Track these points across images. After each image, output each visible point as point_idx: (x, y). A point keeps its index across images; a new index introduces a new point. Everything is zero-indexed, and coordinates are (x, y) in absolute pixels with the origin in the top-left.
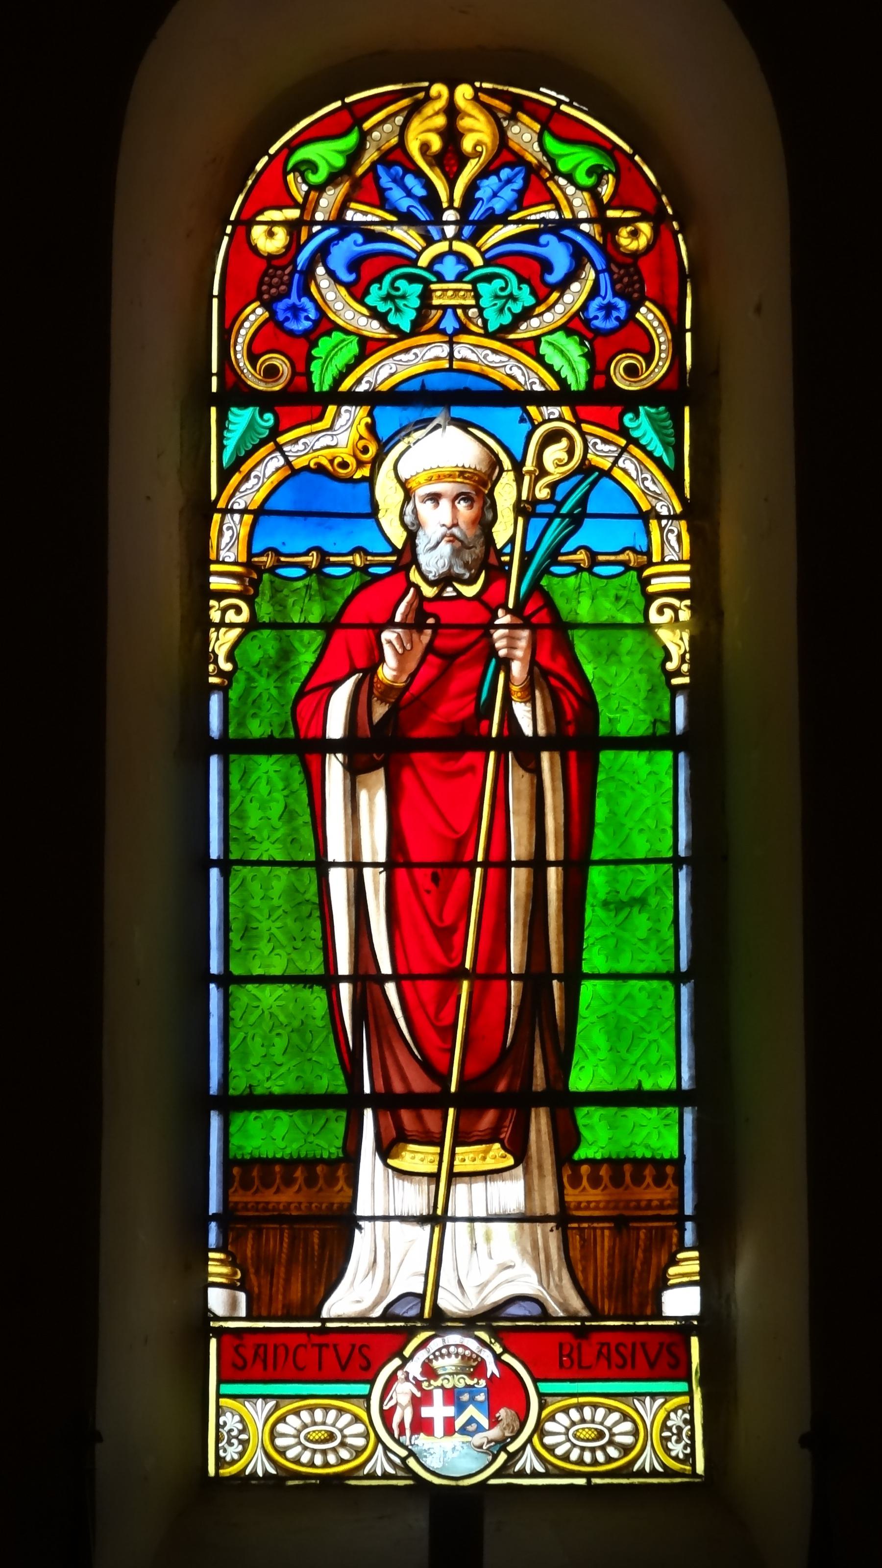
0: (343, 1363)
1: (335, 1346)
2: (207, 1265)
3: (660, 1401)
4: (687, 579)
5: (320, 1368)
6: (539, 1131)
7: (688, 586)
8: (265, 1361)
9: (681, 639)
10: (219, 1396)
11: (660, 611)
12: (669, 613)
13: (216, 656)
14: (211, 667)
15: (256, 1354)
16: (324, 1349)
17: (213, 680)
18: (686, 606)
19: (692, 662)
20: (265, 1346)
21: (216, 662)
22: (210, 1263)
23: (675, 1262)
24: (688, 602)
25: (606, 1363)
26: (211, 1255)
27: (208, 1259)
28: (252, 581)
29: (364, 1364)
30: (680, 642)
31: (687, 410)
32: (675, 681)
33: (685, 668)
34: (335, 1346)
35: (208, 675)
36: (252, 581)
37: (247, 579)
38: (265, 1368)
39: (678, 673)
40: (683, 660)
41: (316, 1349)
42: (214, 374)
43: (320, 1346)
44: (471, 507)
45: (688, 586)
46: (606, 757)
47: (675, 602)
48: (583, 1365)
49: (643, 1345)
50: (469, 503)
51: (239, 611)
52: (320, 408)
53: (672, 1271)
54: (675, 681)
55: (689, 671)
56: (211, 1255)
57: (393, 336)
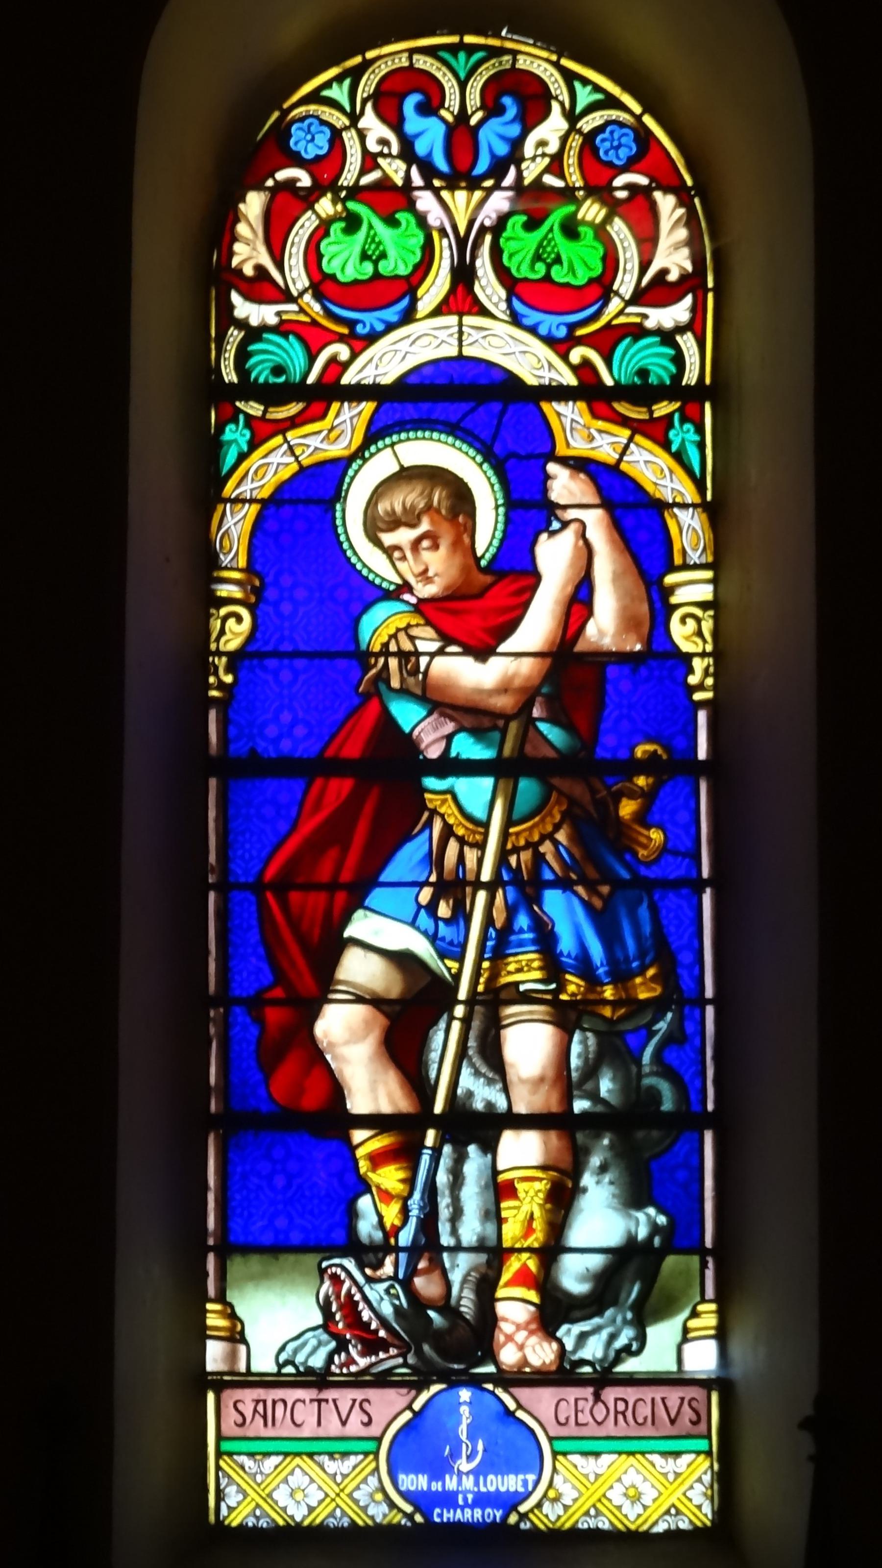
0: (344, 1418)
1: (334, 1401)
2: (205, 1318)
3: (289, 1459)
4: (710, 588)
5: (319, 1423)
6: (298, 358)
8: (265, 1417)
10: (219, 1454)
11: (683, 620)
12: (691, 624)
13: (216, 668)
14: (212, 680)
15: (255, 1411)
16: (323, 1404)
17: (214, 693)
18: (710, 616)
19: (716, 675)
20: (265, 1402)
21: (216, 674)
22: (208, 1315)
24: (711, 613)
25: (261, 1421)
26: (209, 1306)
27: (206, 1311)
28: (254, 588)
29: (694, 1418)
31: (708, 407)
33: (710, 681)
34: (334, 1401)
35: (209, 687)
36: (254, 588)
37: (249, 587)
38: (266, 1424)
39: (701, 687)
40: (706, 673)
41: (316, 1404)
42: (461, 1002)
43: (320, 1401)
46: (623, 467)
47: (698, 612)
51: (239, 619)
52: (325, 381)
54: (698, 696)
56: (209, 1306)
57: (405, 302)
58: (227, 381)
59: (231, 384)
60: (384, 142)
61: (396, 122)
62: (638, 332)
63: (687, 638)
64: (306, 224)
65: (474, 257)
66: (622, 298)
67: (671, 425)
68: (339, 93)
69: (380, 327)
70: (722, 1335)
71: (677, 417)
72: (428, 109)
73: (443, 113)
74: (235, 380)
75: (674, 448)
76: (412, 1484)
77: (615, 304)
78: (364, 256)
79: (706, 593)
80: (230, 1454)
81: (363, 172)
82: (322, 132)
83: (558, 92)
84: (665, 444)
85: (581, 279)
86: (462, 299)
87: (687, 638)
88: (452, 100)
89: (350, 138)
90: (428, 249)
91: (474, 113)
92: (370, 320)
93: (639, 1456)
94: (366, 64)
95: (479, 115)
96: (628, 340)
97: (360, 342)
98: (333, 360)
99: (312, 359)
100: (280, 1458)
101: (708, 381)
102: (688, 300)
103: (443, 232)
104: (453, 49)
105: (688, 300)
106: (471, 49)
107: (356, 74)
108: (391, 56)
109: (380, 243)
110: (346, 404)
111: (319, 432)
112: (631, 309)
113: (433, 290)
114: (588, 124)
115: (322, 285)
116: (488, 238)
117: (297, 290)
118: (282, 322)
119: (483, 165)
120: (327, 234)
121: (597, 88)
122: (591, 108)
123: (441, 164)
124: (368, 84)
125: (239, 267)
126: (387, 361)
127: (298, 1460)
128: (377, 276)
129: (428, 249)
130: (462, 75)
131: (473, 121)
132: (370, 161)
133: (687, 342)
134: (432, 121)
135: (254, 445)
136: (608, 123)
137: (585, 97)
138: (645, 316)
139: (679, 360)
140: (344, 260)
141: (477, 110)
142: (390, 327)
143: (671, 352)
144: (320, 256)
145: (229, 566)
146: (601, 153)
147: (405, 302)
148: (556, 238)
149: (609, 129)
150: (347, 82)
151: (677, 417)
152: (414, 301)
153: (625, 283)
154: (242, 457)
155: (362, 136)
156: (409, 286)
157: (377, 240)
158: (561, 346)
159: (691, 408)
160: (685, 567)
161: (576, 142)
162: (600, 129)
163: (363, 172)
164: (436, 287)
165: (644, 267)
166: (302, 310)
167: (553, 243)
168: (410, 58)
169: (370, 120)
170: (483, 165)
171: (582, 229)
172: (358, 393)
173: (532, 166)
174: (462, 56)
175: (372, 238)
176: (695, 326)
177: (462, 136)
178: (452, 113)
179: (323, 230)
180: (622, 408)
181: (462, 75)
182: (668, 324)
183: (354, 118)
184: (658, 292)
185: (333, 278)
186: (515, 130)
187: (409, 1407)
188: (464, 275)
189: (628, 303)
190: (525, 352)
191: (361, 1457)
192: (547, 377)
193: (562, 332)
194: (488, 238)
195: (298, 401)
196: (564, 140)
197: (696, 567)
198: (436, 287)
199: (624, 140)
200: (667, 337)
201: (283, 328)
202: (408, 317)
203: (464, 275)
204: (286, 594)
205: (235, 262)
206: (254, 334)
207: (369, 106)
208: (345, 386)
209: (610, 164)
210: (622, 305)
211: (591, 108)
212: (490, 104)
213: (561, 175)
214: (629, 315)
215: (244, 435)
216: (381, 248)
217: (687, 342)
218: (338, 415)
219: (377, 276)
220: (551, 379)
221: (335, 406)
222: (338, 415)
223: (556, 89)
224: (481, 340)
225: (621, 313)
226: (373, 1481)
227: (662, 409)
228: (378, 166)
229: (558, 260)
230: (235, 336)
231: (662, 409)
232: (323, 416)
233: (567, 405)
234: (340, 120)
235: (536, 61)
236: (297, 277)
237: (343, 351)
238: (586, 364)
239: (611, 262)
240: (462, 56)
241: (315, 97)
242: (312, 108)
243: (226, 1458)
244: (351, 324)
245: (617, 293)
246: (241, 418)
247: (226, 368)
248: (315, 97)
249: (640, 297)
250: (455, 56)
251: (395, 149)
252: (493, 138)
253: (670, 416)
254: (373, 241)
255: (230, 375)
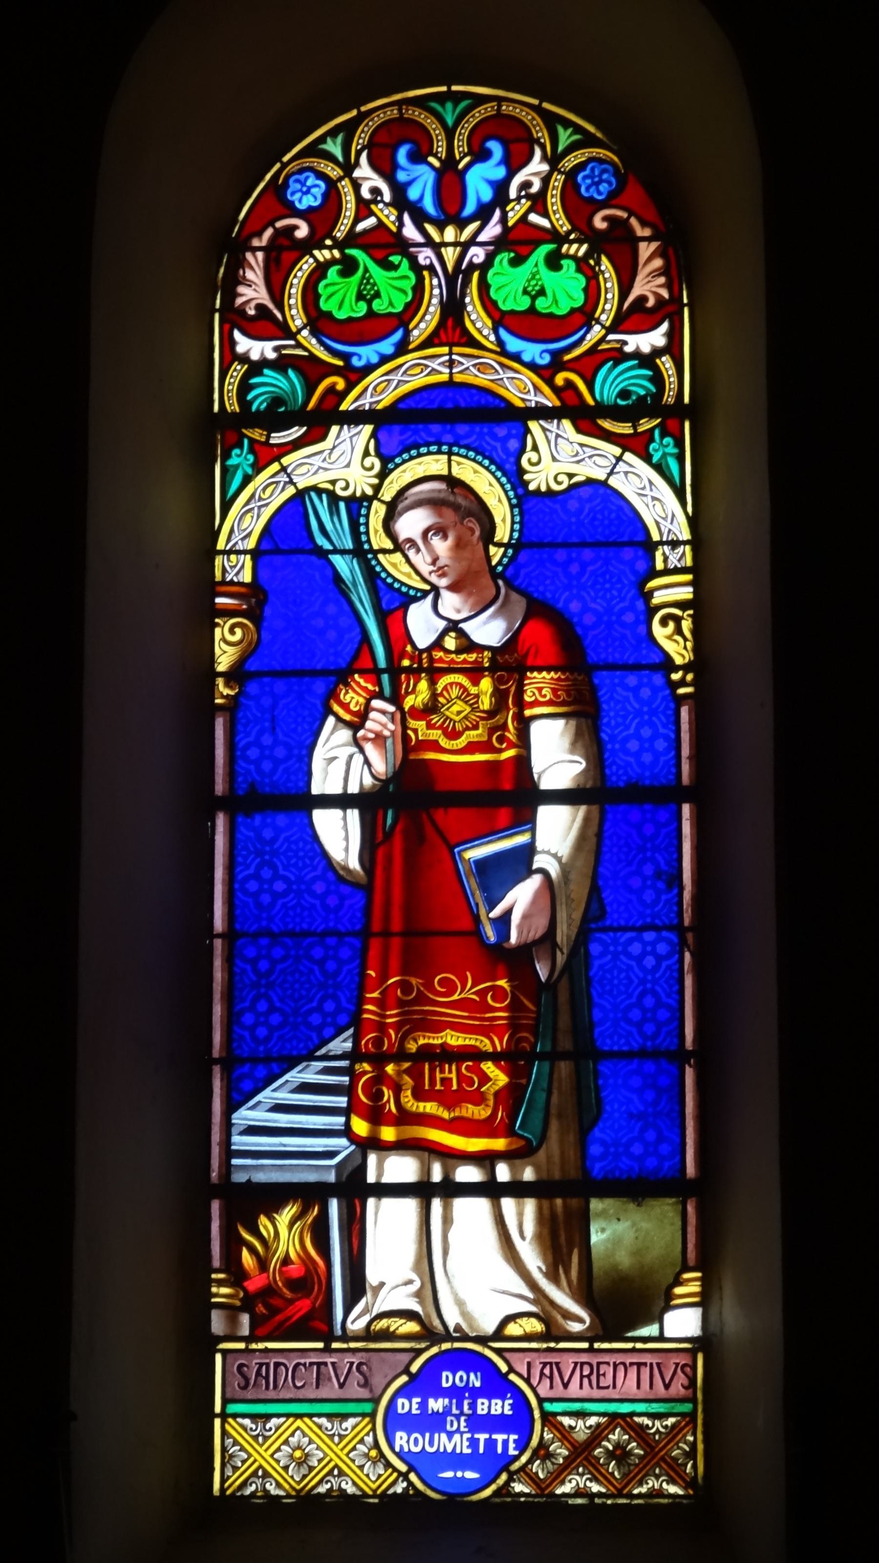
3: (291, 1420)
4: (691, 589)
7: (691, 596)
8: (267, 1378)
9: (685, 648)
15: (542, 1374)
16: (322, 1367)
17: (218, 701)
23: (678, 1282)
30: (684, 652)
32: (682, 691)
39: (683, 683)
41: (635, 1367)
44: (445, 537)
45: (691, 596)
48: (601, 1385)
49: (658, 1364)
50: (441, 534)
53: (678, 1290)
54: (682, 691)
55: (693, 680)
57: (398, 336)
58: (229, 410)
59: (234, 413)
60: (376, 191)
61: (386, 168)
62: (619, 356)
63: (669, 638)
64: (306, 265)
65: (463, 295)
66: (603, 326)
67: (652, 440)
68: (334, 147)
69: (375, 359)
70: (704, 1301)
71: (657, 433)
72: (418, 157)
73: (431, 159)
74: (238, 410)
75: (655, 460)
76: (416, 1440)
77: (597, 331)
78: (360, 297)
79: (686, 593)
80: (235, 1416)
81: (357, 220)
82: (315, 198)
83: (540, 134)
84: (647, 458)
85: (562, 310)
86: (452, 330)
87: (669, 638)
88: (441, 148)
89: (345, 186)
90: (419, 289)
91: (461, 159)
92: (366, 354)
93: (306, 1420)
94: (362, 117)
95: (467, 159)
96: (610, 364)
97: (355, 375)
98: (331, 389)
99: (309, 392)
100: (359, 1419)
101: (687, 400)
102: (665, 327)
103: (431, 268)
104: (440, 98)
105: (665, 327)
106: (457, 97)
107: (349, 129)
108: (381, 108)
109: (375, 284)
110: (345, 427)
111: (321, 452)
112: (611, 337)
113: (422, 325)
114: (570, 162)
115: (320, 322)
116: (476, 275)
117: (296, 326)
118: (281, 357)
119: (470, 207)
120: (324, 276)
121: (578, 129)
122: (571, 148)
123: (429, 205)
124: (361, 138)
125: (242, 308)
126: (380, 390)
127: (299, 1423)
128: (371, 314)
129: (419, 289)
130: (450, 121)
131: (461, 166)
132: (364, 209)
133: (666, 363)
134: (422, 169)
135: (258, 468)
136: (590, 160)
137: (565, 137)
138: (625, 343)
139: (658, 379)
140: (340, 299)
141: (465, 155)
142: (384, 359)
143: (649, 373)
144: (318, 296)
145: (235, 579)
146: (583, 190)
147: (398, 336)
148: (541, 272)
149: (590, 166)
150: (339, 139)
151: (657, 433)
152: (407, 333)
153: (607, 312)
154: (247, 480)
155: (356, 186)
156: (403, 319)
157: (372, 281)
158: (546, 373)
159: (672, 424)
160: (667, 572)
161: (557, 181)
162: (581, 167)
163: (357, 220)
164: (426, 323)
165: (624, 293)
166: (299, 345)
167: (537, 277)
168: (400, 110)
169: (364, 170)
170: (470, 207)
171: (564, 262)
172: (356, 418)
173: (517, 207)
174: (449, 106)
175: (367, 278)
176: (673, 347)
177: (450, 182)
178: (439, 159)
179: (320, 271)
180: (606, 424)
181: (450, 121)
182: (646, 349)
183: (348, 168)
184: (635, 317)
185: (329, 315)
186: (500, 173)
187: (406, 1371)
188: (453, 309)
189: (610, 330)
190: (513, 378)
191: (282, 1420)
192: (533, 399)
193: (546, 359)
194: (476, 275)
195: (301, 425)
196: (546, 181)
197: (676, 571)
198: (426, 323)
199: (605, 176)
200: (647, 360)
201: (281, 364)
202: (402, 348)
203: (453, 309)
204: (267, 752)
205: (239, 301)
206: (257, 367)
207: (364, 155)
208: (343, 411)
209: (591, 199)
210: (603, 332)
211: (571, 148)
212: (476, 148)
213: (545, 214)
214: (609, 342)
215: (248, 460)
216: (376, 288)
217: (666, 363)
218: (338, 437)
219: (371, 314)
220: (537, 402)
221: (335, 429)
222: (338, 437)
223: (537, 132)
224: (471, 368)
225: (602, 340)
226: (369, 1439)
227: (645, 425)
228: (372, 213)
229: (542, 292)
230: (238, 370)
231: (645, 425)
232: (323, 437)
233: (552, 422)
234: (334, 172)
235: (520, 106)
236: (297, 318)
237: (341, 384)
238: (569, 384)
239: (592, 293)
240: (449, 106)
241: (313, 150)
242: (308, 162)
243: (230, 1420)
244: (346, 357)
245: (598, 321)
246: (246, 442)
247: (229, 400)
248: (313, 150)
249: (620, 324)
250: (443, 105)
251: (387, 197)
252: (478, 183)
253: (652, 430)
254: (368, 283)
255: (233, 406)
